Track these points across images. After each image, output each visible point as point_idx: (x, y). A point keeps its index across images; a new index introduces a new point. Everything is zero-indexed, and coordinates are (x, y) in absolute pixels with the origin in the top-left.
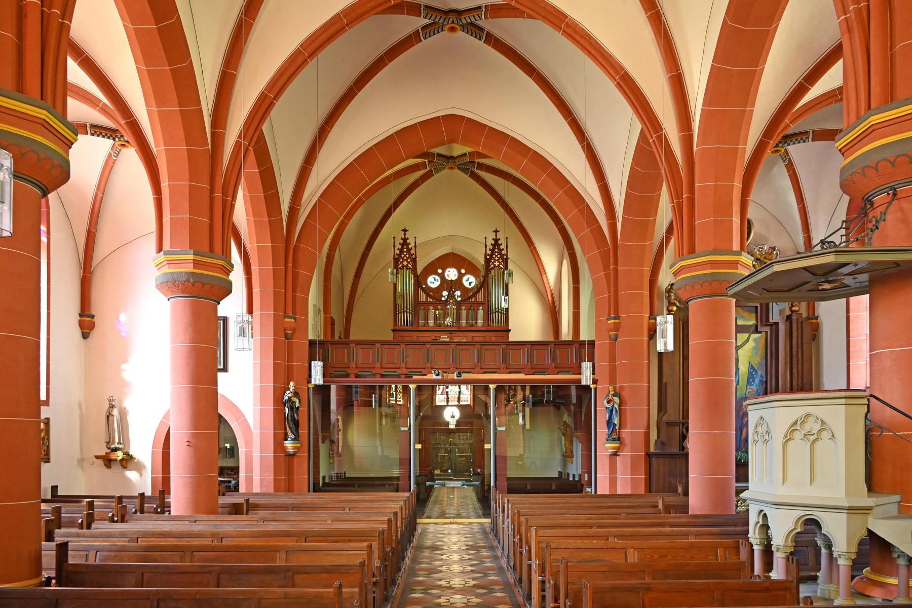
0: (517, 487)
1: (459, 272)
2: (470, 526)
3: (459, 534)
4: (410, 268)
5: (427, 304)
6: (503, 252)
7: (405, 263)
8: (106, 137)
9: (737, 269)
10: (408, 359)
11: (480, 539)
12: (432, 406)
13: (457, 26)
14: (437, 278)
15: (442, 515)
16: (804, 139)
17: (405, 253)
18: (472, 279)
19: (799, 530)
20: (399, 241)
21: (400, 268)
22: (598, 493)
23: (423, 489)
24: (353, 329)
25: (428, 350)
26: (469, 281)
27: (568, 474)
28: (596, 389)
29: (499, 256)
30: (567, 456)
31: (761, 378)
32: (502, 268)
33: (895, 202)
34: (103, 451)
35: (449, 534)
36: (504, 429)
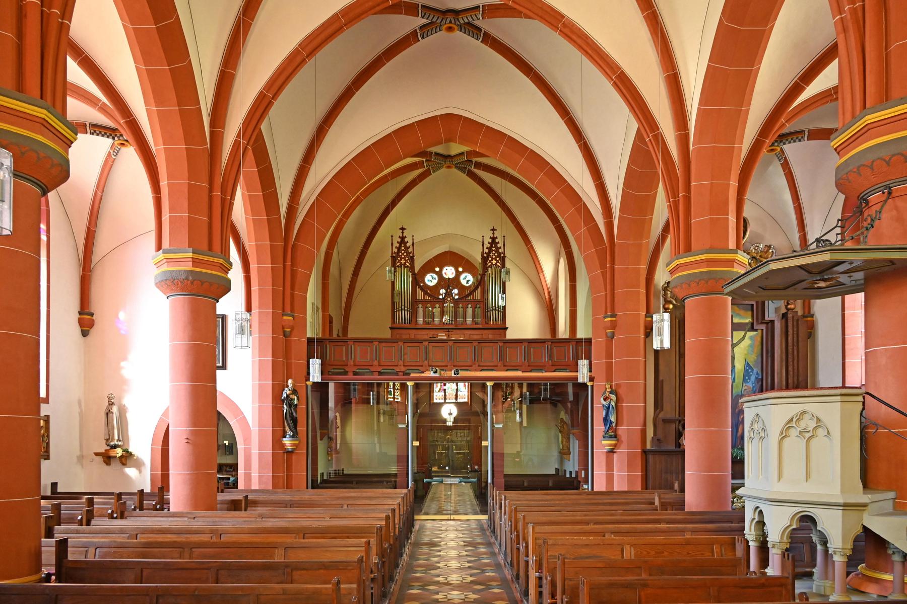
0: (515, 483)
1: (457, 271)
2: (468, 523)
3: (456, 530)
4: (408, 267)
5: (424, 302)
6: (500, 251)
7: (403, 261)
8: (106, 136)
9: (733, 268)
10: (406, 356)
11: (478, 536)
12: (430, 404)
13: (454, 26)
14: (435, 276)
15: (440, 512)
16: (799, 138)
17: (403, 252)
18: (470, 277)
19: (794, 527)
20: (397, 240)
21: (398, 266)
22: (595, 490)
23: (420, 486)
24: (351, 327)
25: (426, 348)
26: (467, 279)
27: (565, 471)
28: (592, 386)
29: (496, 254)
30: (564, 453)
31: (757, 376)
32: (499, 267)
33: (890, 201)
34: (102, 448)
35: (447, 530)
36: (501, 426)
